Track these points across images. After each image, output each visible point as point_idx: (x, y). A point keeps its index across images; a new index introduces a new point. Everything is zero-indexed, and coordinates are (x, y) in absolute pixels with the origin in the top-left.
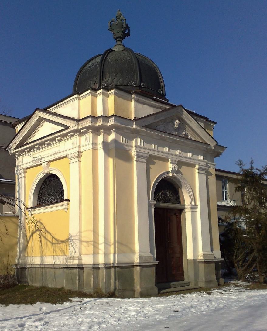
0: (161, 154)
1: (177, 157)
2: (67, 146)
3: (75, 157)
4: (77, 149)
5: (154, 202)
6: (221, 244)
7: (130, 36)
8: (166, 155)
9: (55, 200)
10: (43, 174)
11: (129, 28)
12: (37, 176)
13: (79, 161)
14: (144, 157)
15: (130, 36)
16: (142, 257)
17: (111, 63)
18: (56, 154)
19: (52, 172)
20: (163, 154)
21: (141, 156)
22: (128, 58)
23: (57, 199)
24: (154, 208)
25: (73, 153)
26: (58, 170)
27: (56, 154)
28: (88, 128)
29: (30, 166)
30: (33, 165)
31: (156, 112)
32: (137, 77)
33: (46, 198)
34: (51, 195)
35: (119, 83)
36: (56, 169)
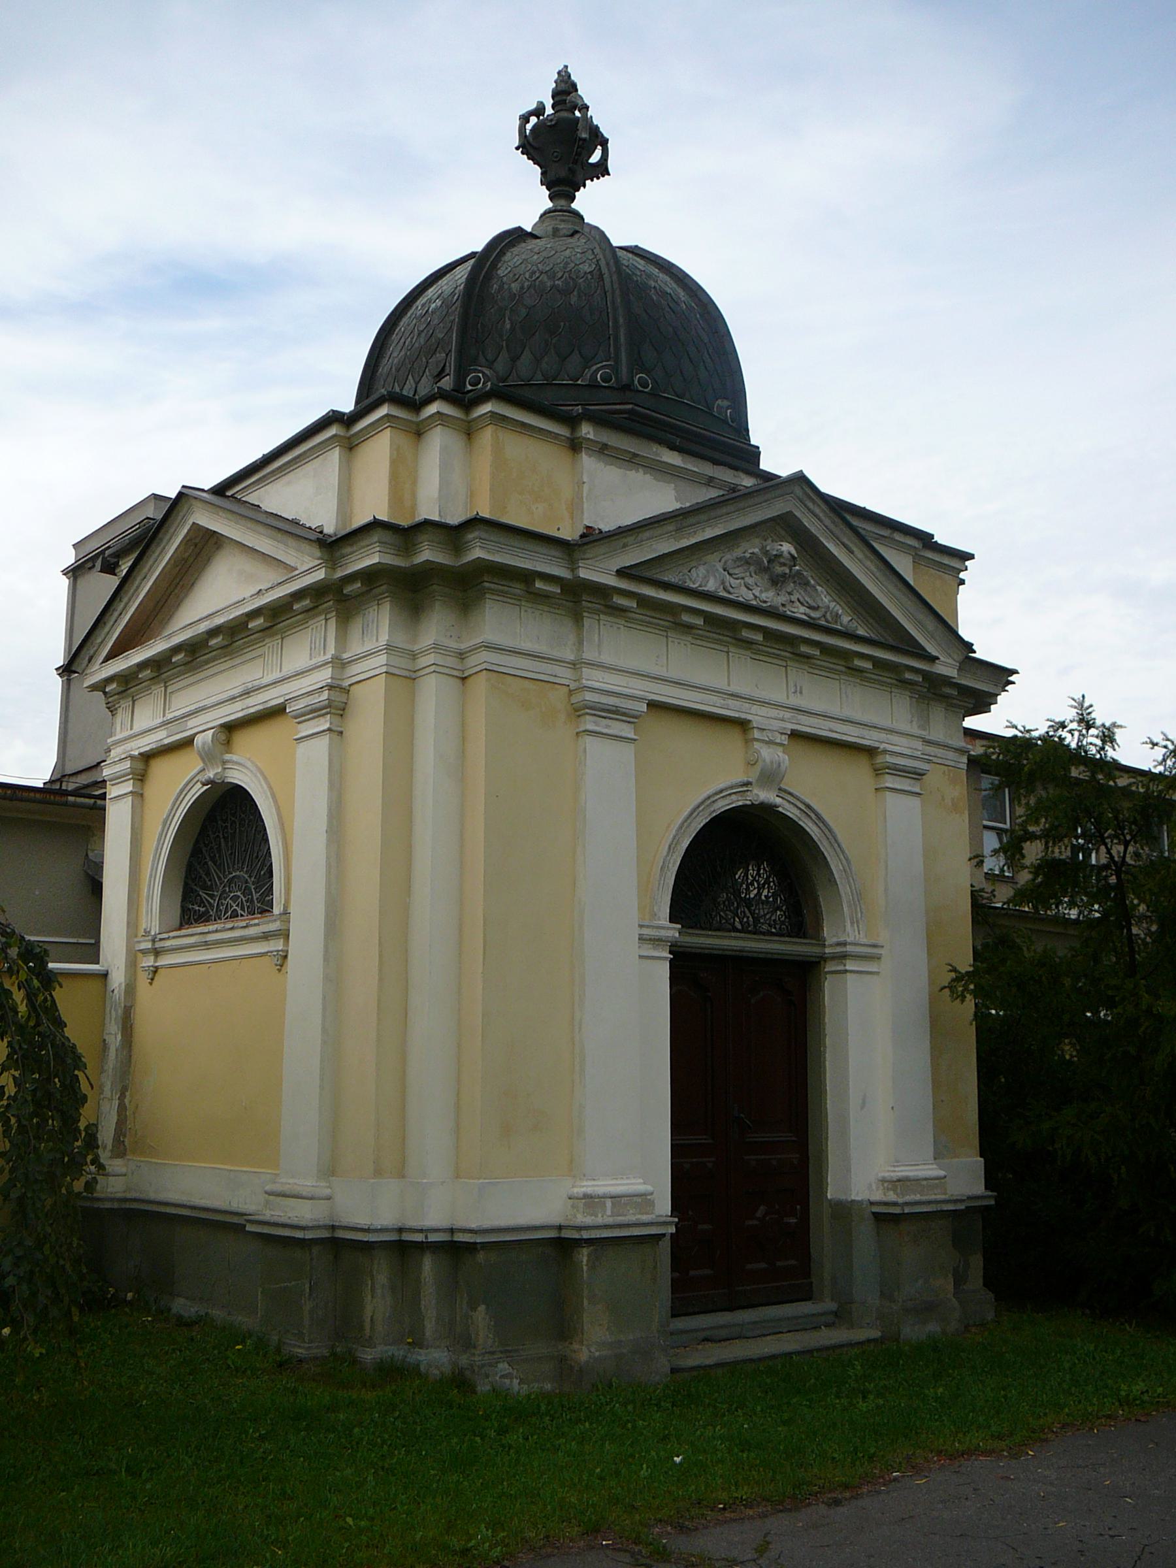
0: (714, 699)
1: (788, 715)
2: (296, 666)
3: (315, 712)
4: (325, 676)
5: (673, 932)
6: (1122, 782)
7: (609, 174)
8: (730, 702)
9: (242, 909)
10: (199, 785)
11: (604, 143)
12: (178, 788)
13: (337, 733)
14: (624, 714)
15: (609, 174)
16: (599, 1197)
17: (513, 285)
18: (247, 693)
19: (237, 777)
20: (720, 702)
21: (609, 711)
22: (586, 268)
23: (252, 901)
24: (671, 961)
25: (309, 693)
26: (257, 766)
27: (247, 693)
28: (370, 576)
29: (154, 746)
30: (166, 742)
31: (688, 505)
32: (617, 349)
33: (212, 896)
34: (231, 881)
35: (539, 375)
36: (249, 764)
